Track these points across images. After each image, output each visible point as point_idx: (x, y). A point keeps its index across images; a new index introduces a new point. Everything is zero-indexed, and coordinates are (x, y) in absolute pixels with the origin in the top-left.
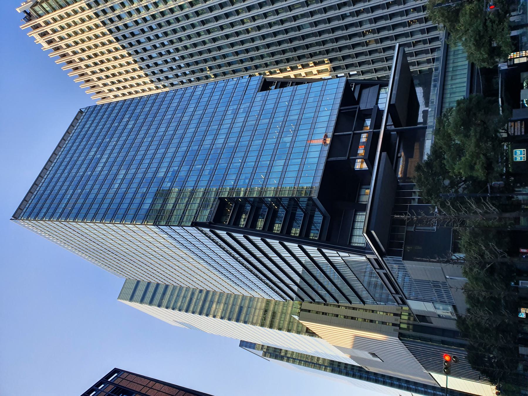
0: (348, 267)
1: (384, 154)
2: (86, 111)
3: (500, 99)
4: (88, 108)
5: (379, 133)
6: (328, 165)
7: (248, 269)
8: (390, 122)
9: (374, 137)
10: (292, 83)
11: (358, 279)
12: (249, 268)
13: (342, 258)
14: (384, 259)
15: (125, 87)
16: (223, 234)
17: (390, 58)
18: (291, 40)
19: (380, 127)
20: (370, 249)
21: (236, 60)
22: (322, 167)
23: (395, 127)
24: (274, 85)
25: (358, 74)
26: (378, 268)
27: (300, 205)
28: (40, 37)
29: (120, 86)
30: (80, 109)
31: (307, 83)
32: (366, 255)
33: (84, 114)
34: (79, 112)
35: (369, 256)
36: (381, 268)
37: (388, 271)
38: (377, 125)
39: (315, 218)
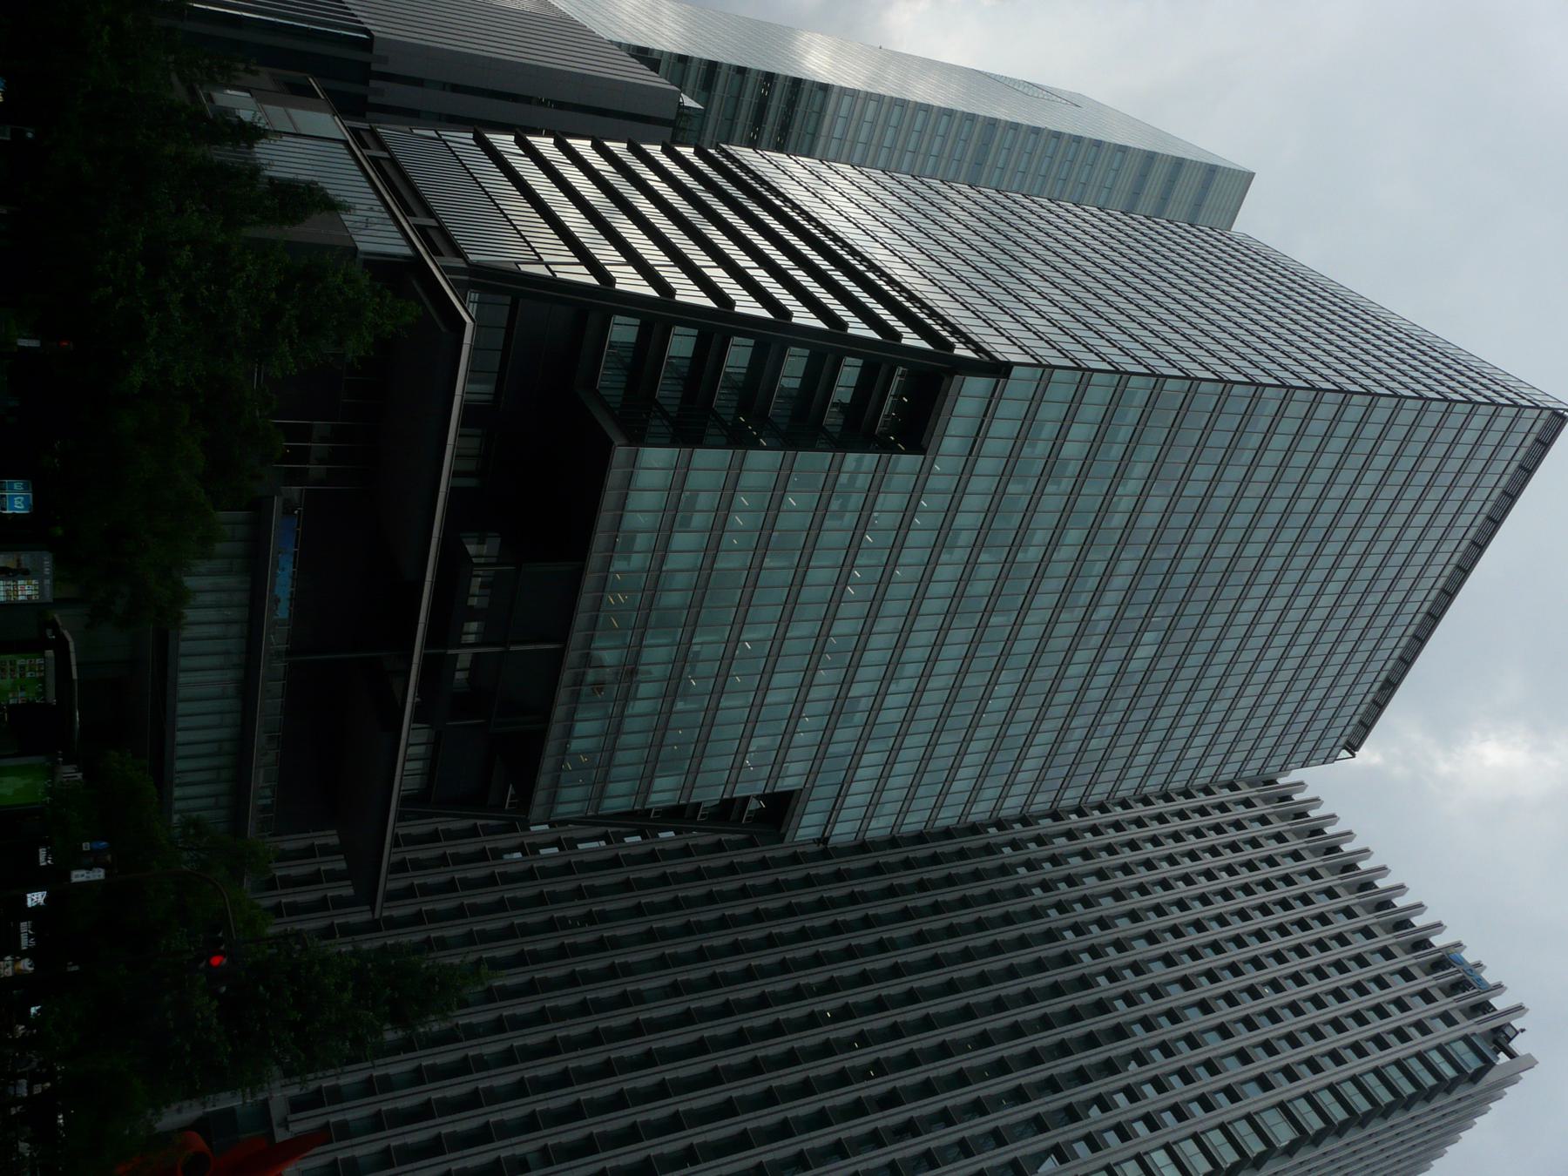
2: (1336, 750)
3: (75, 676)
4: (1330, 759)
5: (428, 643)
9: (442, 632)
11: (493, 201)
13: (541, 259)
14: (407, 251)
15: (1234, 847)
16: (911, 339)
18: (701, 955)
19: (426, 659)
20: (454, 285)
21: (915, 977)
25: (498, 854)
27: (666, 423)
28: (1469, 979)
29: (1266, 872)
30: (1354, 756)
32: (464, 266)
33: (1343, 741)
34: (1356, 748)
35: (459, 263)
36: (422, 231)
37: (358, 153)
38: (434, 669)
39: (623, 385)
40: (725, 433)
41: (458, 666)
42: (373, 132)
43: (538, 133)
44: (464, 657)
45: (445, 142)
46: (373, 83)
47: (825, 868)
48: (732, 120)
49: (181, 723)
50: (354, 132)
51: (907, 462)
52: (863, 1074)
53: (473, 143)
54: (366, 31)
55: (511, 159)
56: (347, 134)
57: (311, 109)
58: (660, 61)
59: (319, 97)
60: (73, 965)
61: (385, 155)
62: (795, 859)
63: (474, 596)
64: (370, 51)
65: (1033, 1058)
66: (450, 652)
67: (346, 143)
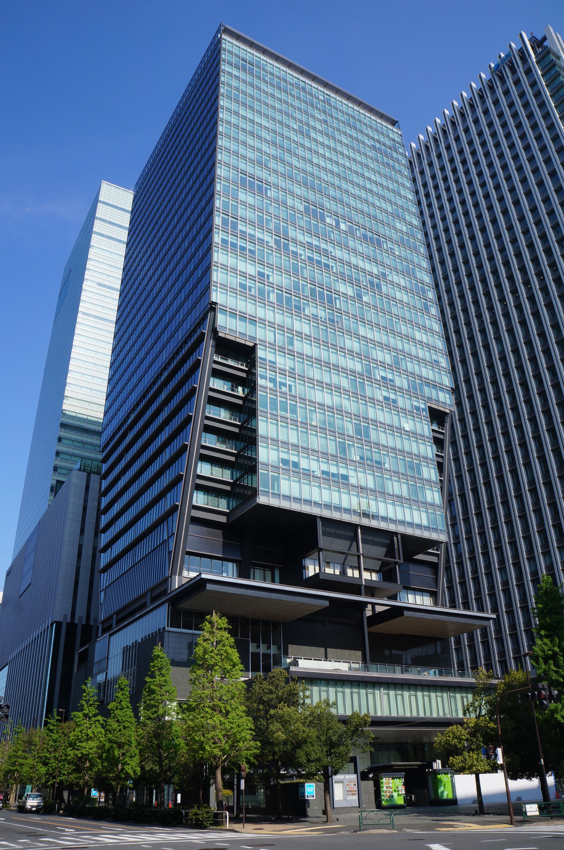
0: (107, 585)
1: (326, 603)
5: (360, 594)
6: (311, 519)
7: (158, 378)
8: (379, 609)
10: (442, 457)
12: (148, 394)
17: (481, 609)
22: (306, 509)
23: (368, 617)
24: (439, 428)
26: (119, 618)
27: (246, 476)
31: (441, 481)
36: (154, 599)
37: (115, 629)
40: (250, 446)
41: (370, 579)
42: (103, 623)
43: (558, 638)
44: (366, 575)
45: (106, 587)
46: (76, 621)
47: (464, 388)
48: (84, 443)
49: (428, 715)
50: (104, 632)
51: (260, 353)
52: (529, 289)
53: (106, 573)
54: (52, 625)
55: (114, 555)
56: (105, 635)
57: (94, 652)
58: (57, 480)
59: (87, 648)
60: (540, 762)
61: (115, 616)
62: (459, 404)
63: (334, 571)
64: (61, 622)
65: (539, 223)
66: (364, 583)
67: (111, 635)
